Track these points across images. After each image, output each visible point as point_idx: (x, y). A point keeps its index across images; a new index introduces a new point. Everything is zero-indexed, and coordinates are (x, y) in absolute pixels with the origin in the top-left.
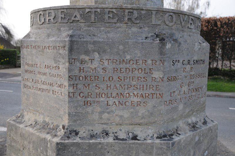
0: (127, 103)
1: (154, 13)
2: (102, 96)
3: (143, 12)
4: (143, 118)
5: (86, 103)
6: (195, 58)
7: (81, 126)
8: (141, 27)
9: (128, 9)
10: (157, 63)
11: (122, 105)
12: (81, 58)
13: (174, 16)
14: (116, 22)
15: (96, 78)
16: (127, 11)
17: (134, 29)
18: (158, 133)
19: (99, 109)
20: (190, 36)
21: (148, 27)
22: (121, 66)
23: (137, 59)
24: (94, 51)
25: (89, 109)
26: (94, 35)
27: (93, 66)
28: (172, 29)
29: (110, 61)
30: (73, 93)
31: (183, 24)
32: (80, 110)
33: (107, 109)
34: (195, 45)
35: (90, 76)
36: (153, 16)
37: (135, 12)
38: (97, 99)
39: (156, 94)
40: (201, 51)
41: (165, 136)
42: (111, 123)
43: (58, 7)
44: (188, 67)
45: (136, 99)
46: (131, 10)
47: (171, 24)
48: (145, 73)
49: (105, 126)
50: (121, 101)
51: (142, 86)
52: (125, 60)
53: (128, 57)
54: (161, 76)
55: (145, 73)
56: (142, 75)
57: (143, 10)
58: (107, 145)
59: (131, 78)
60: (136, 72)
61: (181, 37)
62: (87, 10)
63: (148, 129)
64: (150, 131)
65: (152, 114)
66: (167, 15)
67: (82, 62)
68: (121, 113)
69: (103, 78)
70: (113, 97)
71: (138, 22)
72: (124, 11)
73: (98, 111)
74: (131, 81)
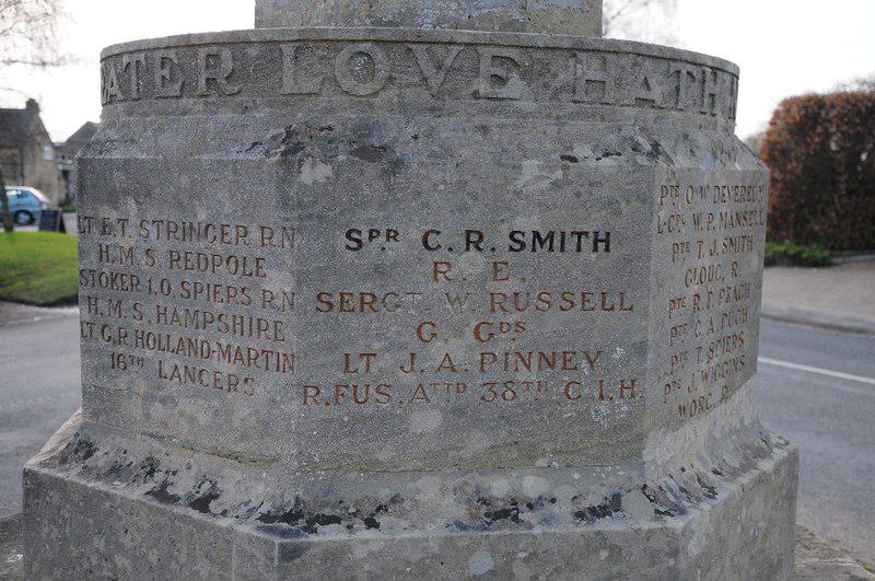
0: (205, 375)
1: (288, 50)
2: (148, 344)
3: (253, 51)
4: (243, 437)
5: (117, 360)
6: (528, 223)
7: (107, 431)
8: (246, 107)
9: (205, 45)
10: (275, 241)
11: (193, 381)
12: (101, 216)
13: (379, 55)
14: (178, 93)
15: (368, 299)
16: (202, 53)
17: (226, 116)
18: (278, 503)
19: (142, 386)
20: (484, 129)
21: (269, 104)
22: (187, 245)
23: (224, 222)
24: (126, 193)
25: (122, 382)
26: (133, 141)
27: (126, 243)
28: (371, 106)
29: (583, 238)
30: (365, 358)
31: (435, 82)
32: (104, 381)
33: (159, 388)
34: (517, 167)
35: (122, 275)
36: (287, 62)
37: (226, 53)
38: (137, 353)
39: (275, 355)
40: (578, 195)
41: (290, 518)
42: (171, 437)
43: (201, 36)
44: (471, 263)
45: (226, 367)
46: (215, 49)
47: (365, 89)
48: (244, 274)
49: (156, 444)
50: (190, 367)
51: (238, 320)
52: (195, 225)
53: (203, 216)
54: (288, 289)
55: (244, 274)
56: (234, 280)
57: (250, 43)
58: (122, 506)
59: (212, 287)
60: (222, 268)
61: (416, 137)
62: (125, 59)
63: (258, 479)
64: (260, 488)
65: (266, 424)
66: (345, 53)
67: (105, 229)
68: (190, 409)
69: (148, 285)
70: (173, 351)
71: (237, 89)
72: (196, 54)
73: (141, 391)
74: (212, 299)
